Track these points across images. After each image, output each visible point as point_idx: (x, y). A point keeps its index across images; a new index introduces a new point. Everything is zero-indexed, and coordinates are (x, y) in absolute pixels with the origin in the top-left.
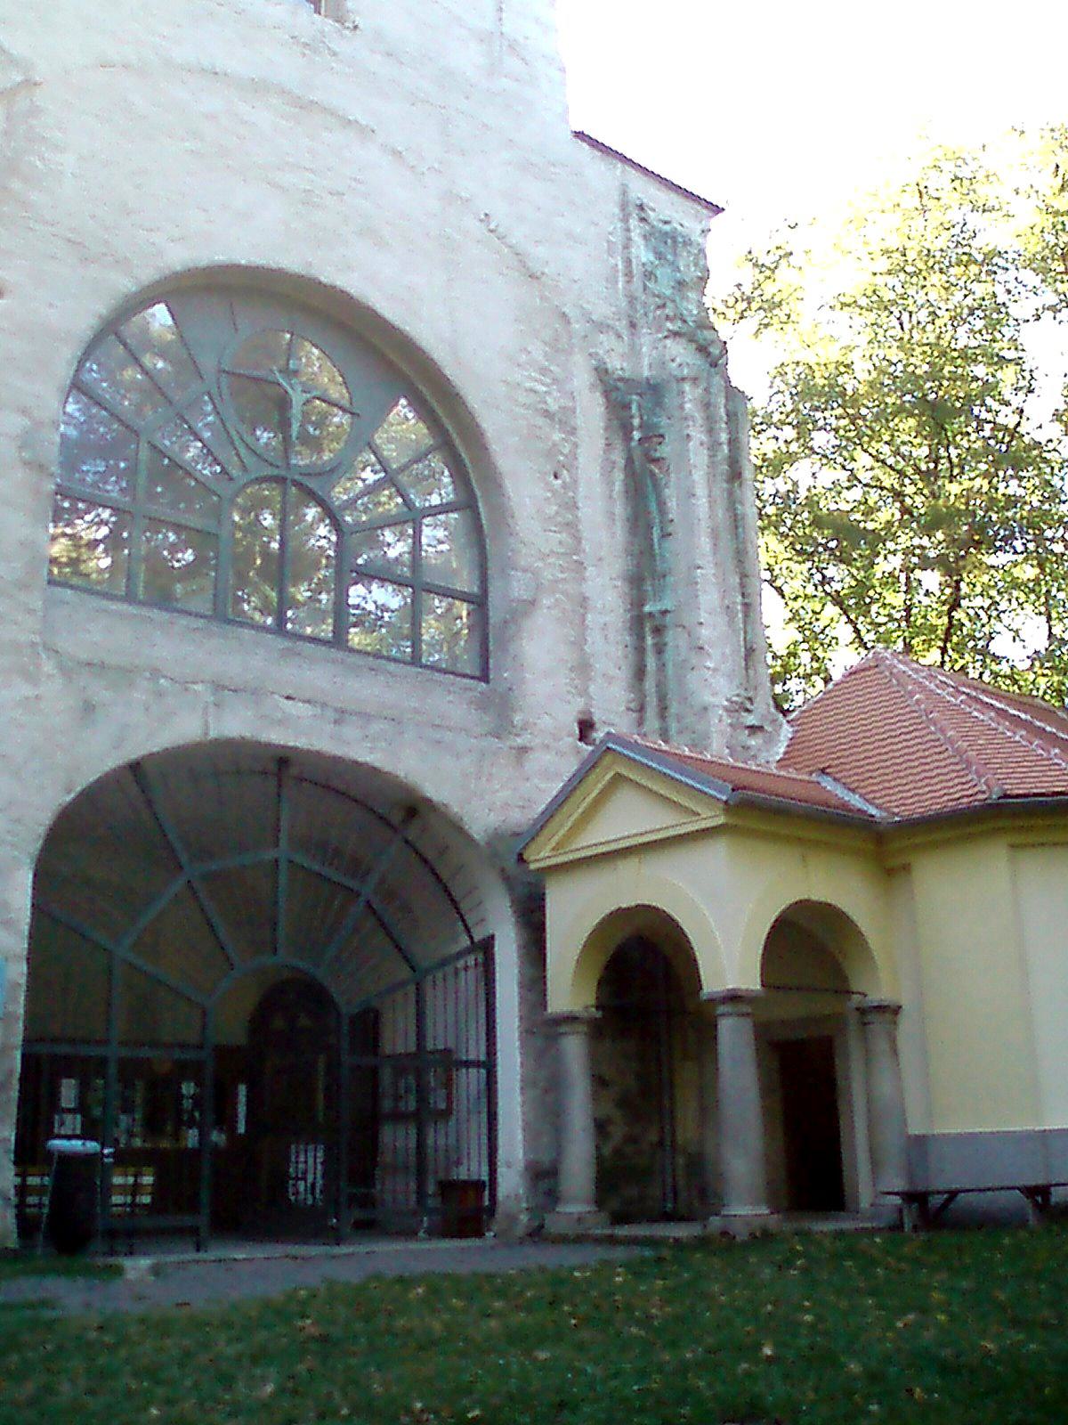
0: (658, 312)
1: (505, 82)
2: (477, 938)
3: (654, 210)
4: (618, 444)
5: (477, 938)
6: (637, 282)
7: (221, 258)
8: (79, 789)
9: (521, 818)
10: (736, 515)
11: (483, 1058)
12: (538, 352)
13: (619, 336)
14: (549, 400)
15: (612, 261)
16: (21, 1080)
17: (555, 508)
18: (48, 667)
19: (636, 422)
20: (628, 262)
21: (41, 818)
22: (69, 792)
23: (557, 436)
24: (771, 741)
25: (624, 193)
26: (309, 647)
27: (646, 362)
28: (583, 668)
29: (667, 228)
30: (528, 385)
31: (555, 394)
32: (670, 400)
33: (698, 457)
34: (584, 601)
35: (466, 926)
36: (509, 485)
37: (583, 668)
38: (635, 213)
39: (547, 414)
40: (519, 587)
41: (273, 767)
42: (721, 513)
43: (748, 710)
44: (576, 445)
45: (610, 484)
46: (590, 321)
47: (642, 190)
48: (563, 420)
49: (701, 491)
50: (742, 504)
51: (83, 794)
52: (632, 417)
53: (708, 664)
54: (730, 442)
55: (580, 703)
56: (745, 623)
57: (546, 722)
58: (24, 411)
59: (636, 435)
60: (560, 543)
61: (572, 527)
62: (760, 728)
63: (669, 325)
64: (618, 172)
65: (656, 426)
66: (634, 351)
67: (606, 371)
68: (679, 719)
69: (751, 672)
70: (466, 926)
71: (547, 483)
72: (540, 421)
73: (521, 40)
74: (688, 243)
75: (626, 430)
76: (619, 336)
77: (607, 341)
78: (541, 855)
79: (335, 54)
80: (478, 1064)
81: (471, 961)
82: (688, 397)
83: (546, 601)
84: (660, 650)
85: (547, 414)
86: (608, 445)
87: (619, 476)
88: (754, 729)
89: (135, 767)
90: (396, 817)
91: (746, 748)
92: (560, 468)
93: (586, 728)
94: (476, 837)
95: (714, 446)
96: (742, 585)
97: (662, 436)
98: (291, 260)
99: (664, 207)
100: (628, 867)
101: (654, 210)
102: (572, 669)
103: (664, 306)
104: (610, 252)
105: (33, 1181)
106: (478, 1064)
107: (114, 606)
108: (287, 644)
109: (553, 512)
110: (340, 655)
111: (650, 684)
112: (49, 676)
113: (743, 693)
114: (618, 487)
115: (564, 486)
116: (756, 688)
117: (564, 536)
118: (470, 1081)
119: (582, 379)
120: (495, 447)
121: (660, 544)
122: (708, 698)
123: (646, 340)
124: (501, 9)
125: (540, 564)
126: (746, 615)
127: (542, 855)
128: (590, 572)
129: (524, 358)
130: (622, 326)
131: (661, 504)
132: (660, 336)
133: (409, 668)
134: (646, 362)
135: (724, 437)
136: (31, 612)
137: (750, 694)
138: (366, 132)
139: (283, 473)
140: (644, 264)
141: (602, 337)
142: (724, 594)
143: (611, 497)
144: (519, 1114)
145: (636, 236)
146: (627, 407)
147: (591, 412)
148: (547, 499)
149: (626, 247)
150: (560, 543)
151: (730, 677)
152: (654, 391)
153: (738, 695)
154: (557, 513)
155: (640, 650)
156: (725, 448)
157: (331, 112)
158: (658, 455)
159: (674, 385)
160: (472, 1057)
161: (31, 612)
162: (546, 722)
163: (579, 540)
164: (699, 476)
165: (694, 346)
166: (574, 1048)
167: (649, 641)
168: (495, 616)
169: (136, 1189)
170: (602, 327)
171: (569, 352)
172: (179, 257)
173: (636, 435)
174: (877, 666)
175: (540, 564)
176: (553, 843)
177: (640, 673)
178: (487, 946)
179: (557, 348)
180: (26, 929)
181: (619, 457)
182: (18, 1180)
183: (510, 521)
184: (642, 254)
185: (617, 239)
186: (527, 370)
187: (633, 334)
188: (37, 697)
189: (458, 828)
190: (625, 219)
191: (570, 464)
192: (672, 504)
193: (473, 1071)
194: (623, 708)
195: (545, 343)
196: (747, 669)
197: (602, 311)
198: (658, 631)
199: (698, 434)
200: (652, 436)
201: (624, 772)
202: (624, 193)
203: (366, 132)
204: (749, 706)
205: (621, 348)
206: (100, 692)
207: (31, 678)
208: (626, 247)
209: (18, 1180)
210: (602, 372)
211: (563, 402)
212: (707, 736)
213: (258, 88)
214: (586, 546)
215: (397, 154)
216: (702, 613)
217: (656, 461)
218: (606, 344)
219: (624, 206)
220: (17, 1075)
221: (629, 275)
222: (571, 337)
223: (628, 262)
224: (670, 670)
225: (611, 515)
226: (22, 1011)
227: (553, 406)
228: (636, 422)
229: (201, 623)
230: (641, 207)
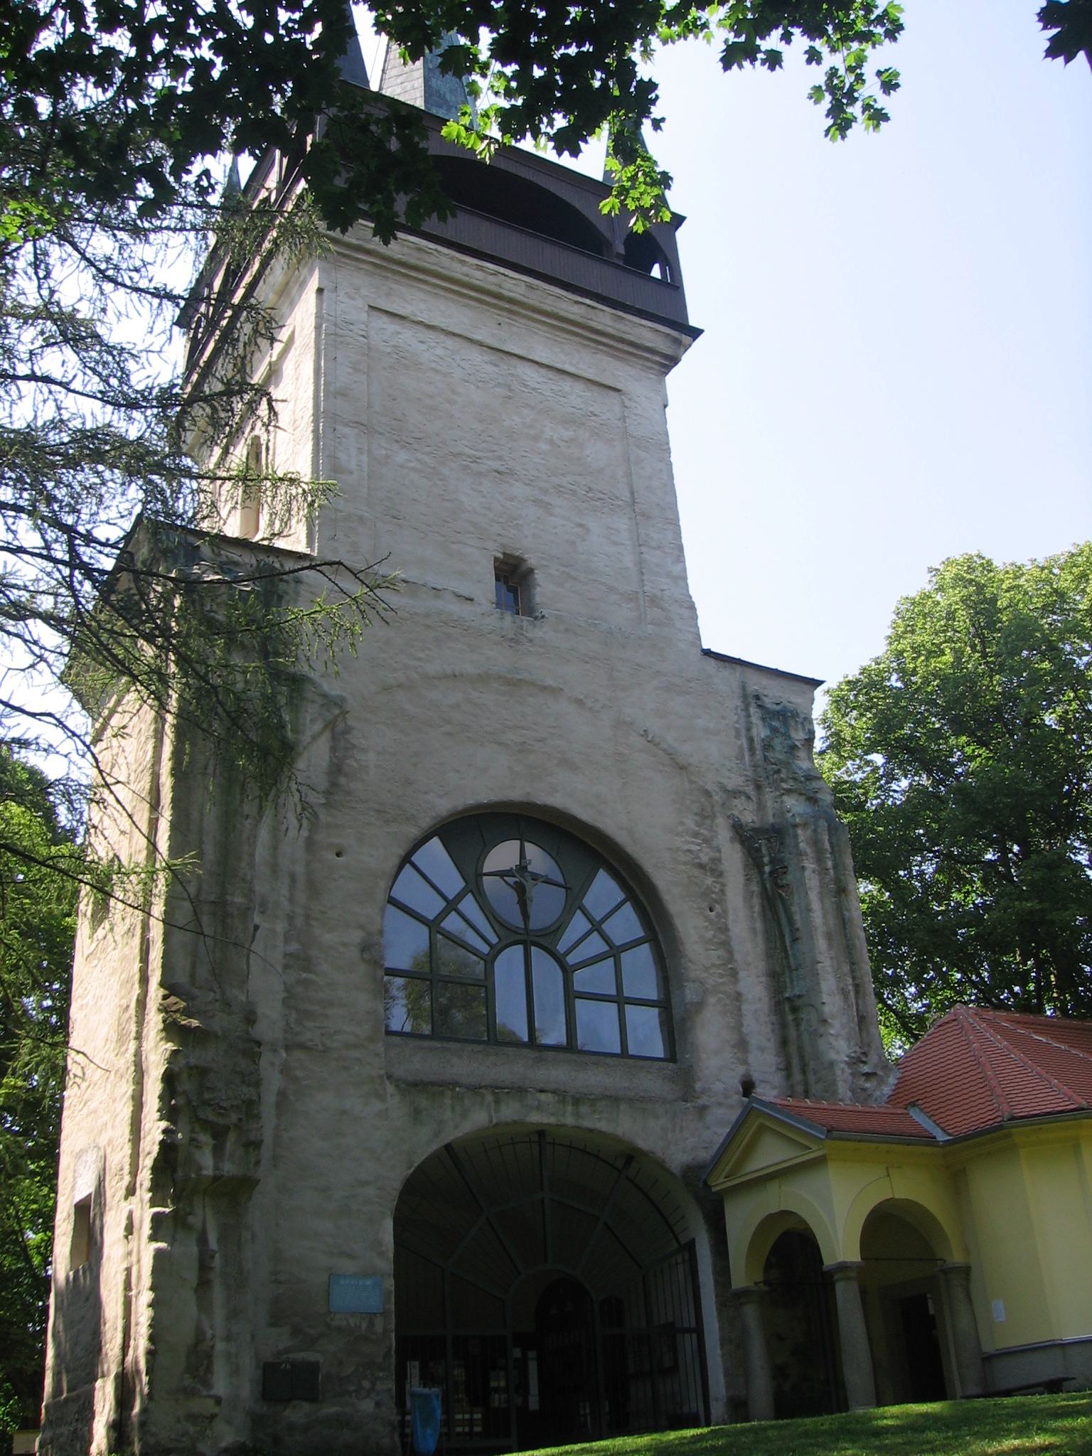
0: (775, 776)
1: (650, 629)
2: (683, 1241)
3: (766, 696)
4: (756, 878)
5: (683, 1241)
6: (759, 753)
7: (471, 801)
8: (416, 1165)
9: (704, 1155)
10: (844, 919)
11: (693, 1324)
12: (690, 822)
13: (748, 798)
14: (701, 855)
15: (739, 742)
16: (155, 1169)
17: (712, 932)
18: (390, 1088)
19: (766, 860)
20: (751, 740)
21: (396, 1177)
22: (410, 1168)
23: (709, 880)
24: (882, 1081)
25: (744, 688)
26: (550, 1054)
27: (770, 813)
28: (742, 1045)
29: (778, 708)
30: (686, 847)
31: (705, 850)
32: (789, 841)
33: (812, 881)
34: (738, 996)
35: (674, 1234)
36: (678, 923)
37: (742, 1045)
38: (753, 702)
39: (701, 866)
40: (690, 994)
41: (535, 1138)
42: (832, 921)
43: (864, 1063)
44: (723, 885)
45: (751, 907)
46: (726, 791)
47: (756, 683)
48: (714, 869)
49: (816, 905)
50: (848, 910)
51: (419, 1167)
52: (762, 857)
53: (832, 1032)
54: (835, 867)
55: (741, 1070)
56: (857, 998)
57: (718, 1086)
58: (361, 927)
59: (767, 869)
60: (719, 957)
61: (726, 945)
62: (875, 1074)
63: (784, 785)
64: (738, 674)
65: (782, 860)
66: (761, 807)
67: (741, 826)
68: (815, 1072)
69: (864, 1034)
70: (674, 1234)
71: (706, 917)
72: (696, 872)
73: (659, 594)
74: (795, 715)
75: (758, 865)
76: (748, 798)
77: (740, 803)
78: (719, 1183)
79: (531, 641)
80: (690, 1331)
81: (679, 1259)
82: (801, 838)
83: (712, 1000)
84: (797, 1022)
85: (701, 866)
86: (748, 880)
87: (756, 901)
88: (868, 1075)
89: (448, 1147)
90: (620, 1164)
91: (864, 1090)
92: (714, 902)
93: (748, 1087)
94: (675, 1172)
95: (823, 871)
96: (852, 971)
97: (786, 867)
98: (516, 793)
99: (775, 693)
100: (773, 1188)
101: (766, 696)
102: (734, 1046)
103: (778, 771)
104: (738, 736)
105: (1077, 1434)
106: (690, 1331)
107: (427, 1044)
108: (536, 1054)
109: (711, 937)
110: (574, 1057)
111: (793, 1049)
112: (392, 1095)
113: (858, 1050)
114: (757, 908)
115: (718, 916)
116: (869, 1045)
117: (720, 952)
118: (689, 1341)
119: (724, 833)
120: (666, 897)
121: (791, 946)
122: (832, 1055)
123: (769, 796)
124: (642, 573)
125: (705, 975)
126: (857, 993)
127: (718, 1182)
128: (742, 974)
129: (680, 828)
130: (750, 789)
131: (791, 921)
132: (778, 793)
133: (621, 1060)
134: (770, 813)
135: (830, 864)
136: (377, 1055)
137: (865, 1049)
138: (555, 692)
139: (525, 937)
140: (763, 740)
141: (736, 801)
142: (839, 979)
143: (752, 917)
144: (720, 1363)
145: (755, 719)
146: (759, 850)
147: (733, 858)
148: (706, 927)
149: (749, 729)
150: (719, 957)
151: (848, 1040)
152: (778, 833)
153: (855, 1052)
154: (714, 936)
155: (783, 1025)
156: (831, 871)
157: (533, 684)
158: (784, 882)
159: (791, 831)
160: (686, 1325)
161: (377, 1055)
162: (718, 1086)
163: (730, 952)
164: (814, 897)
165: (804, 797)
166: (751, 1313)
167: (790, 1017)
168: (677, 1012)
169: (471, 1422)
170: (736, 793)
171: (714, 817)
172: (444, 806)
173: (767, 869)
174: (387, 688)
175: (705, 975)
176: (724, 1174)
177: (784, 1042)
178: (691, 1247)
179: (705, 816)
180: (391, 1255)
181: (755, 888)
182: (399, 1418)
183: (681, 947)
184: (760, 731)
185: (741, 726)
186: (683, 836)
187: (759, 794)
188: (387, 1109)
189: (661, 1165)
190: (746, 709)
191: (721, 900)
192: (797, 917)
193: (687, 1336)
194: (774, 1069)
195: (696, 814)
196: (860, 1030)
197: (734, 781)
198: (795, 1010)
199: (810, 865)
200: (779, 869)
201: (768, 1123)
202: (744, 688)
203: (555, 692)
204: (864, 1059)
205: (752, 806)
206: (423, 1102)
207: (381, 1097)
208: (749, 729)
209: (399, 1418)
210: (738, 828)
211: (712, 854)
212: (834, 1083)
213: (483, 679)
214: (737, 956)
215: (580, 703)
216: (824, 996)
217: (782, 887)
218: (739, 805)
219: (745, 696)
220: (394, 1348)
221: (752, 750)
222: (713, 806)
223: (751, 740)
224: (806, 1037)
225: (754, 930)
226: (393, 1307)
227: (705, 859)
228: (766, 860)
229: (481, 1047)
230: (757, 697)
